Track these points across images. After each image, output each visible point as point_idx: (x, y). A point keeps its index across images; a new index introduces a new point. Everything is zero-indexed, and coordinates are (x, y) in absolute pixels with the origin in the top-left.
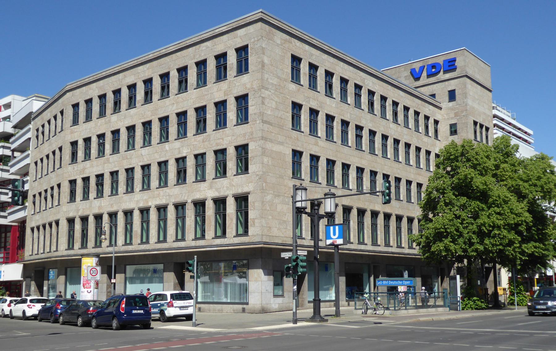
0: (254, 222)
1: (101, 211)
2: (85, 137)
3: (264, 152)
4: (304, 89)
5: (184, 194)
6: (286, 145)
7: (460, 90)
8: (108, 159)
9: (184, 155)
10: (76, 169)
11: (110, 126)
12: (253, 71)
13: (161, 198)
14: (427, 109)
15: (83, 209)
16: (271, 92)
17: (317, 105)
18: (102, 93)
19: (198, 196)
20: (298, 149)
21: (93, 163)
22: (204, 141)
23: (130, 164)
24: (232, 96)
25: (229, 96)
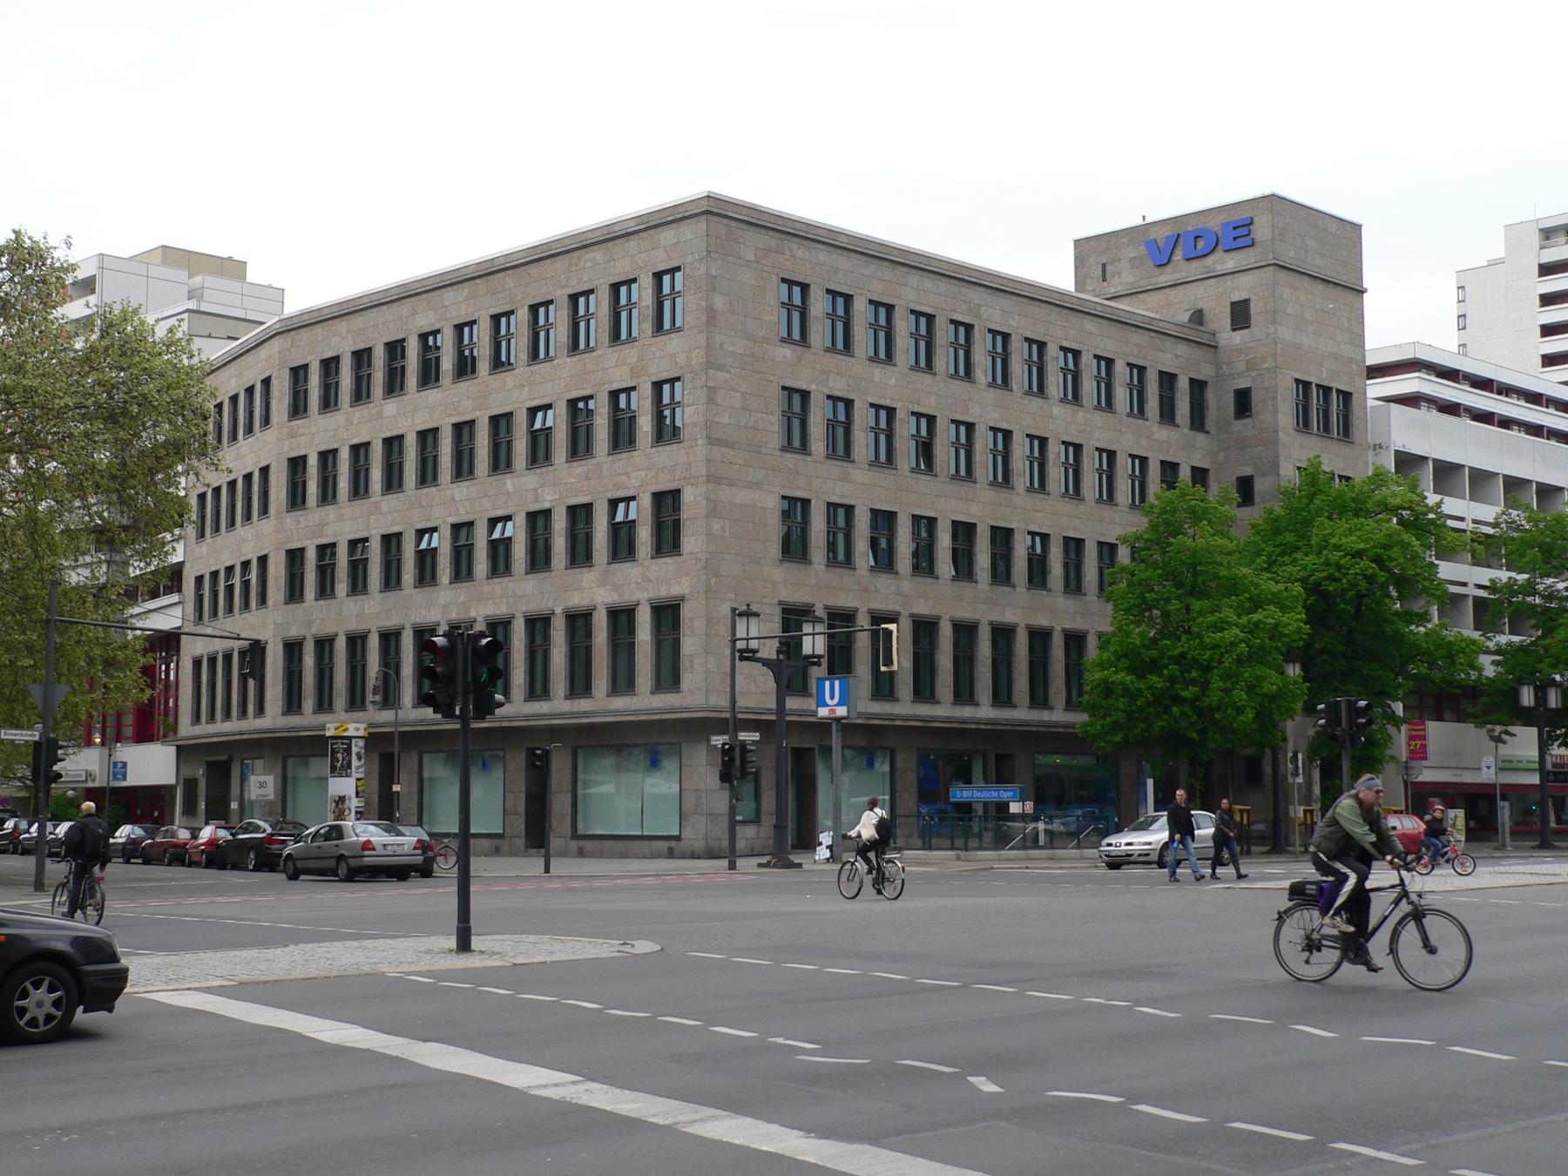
0: (692, 662)
1: (364, 626)
2: (324, 447)
3: (713, 510)
4: (814, 354)
5: (547, 595)
6: (766, 487)
7: (1261, 304)
8: (377, 505)
9: (547, 505)
10: (303, 523)
11: (381, 427)
12: (691, 328)
13: (496, 600)
14: (1170, 356)
15: (323, 620)
16: (730, 372)
17: (846, 388)
18: (362, 346)
19: (577, 601)
20: (798, 494)
21: (342, 511)
22: (590, 476)
23: (428, 520)
24: (647, 379)
25: (641, 380)
